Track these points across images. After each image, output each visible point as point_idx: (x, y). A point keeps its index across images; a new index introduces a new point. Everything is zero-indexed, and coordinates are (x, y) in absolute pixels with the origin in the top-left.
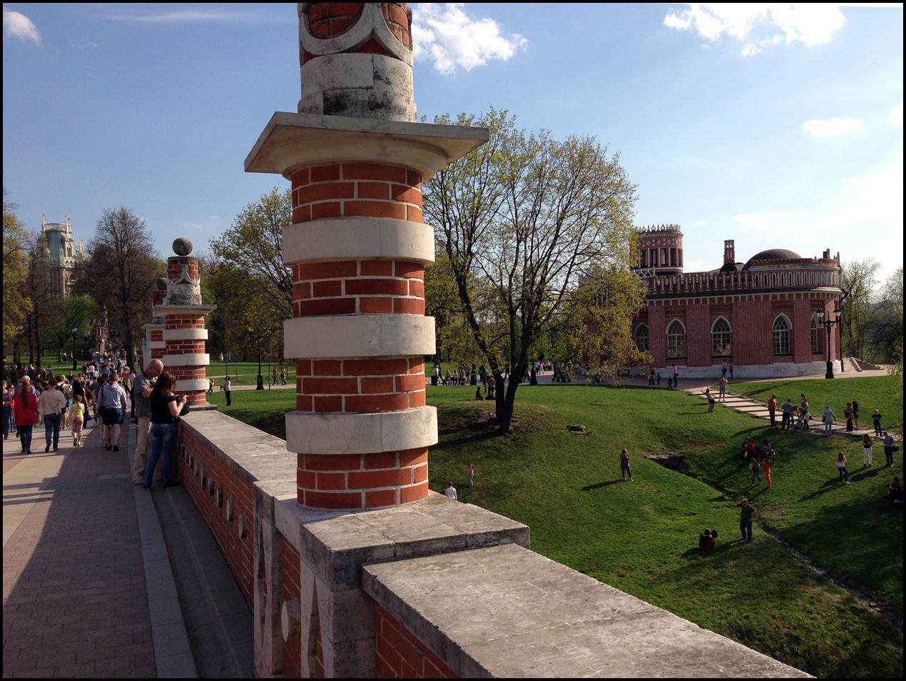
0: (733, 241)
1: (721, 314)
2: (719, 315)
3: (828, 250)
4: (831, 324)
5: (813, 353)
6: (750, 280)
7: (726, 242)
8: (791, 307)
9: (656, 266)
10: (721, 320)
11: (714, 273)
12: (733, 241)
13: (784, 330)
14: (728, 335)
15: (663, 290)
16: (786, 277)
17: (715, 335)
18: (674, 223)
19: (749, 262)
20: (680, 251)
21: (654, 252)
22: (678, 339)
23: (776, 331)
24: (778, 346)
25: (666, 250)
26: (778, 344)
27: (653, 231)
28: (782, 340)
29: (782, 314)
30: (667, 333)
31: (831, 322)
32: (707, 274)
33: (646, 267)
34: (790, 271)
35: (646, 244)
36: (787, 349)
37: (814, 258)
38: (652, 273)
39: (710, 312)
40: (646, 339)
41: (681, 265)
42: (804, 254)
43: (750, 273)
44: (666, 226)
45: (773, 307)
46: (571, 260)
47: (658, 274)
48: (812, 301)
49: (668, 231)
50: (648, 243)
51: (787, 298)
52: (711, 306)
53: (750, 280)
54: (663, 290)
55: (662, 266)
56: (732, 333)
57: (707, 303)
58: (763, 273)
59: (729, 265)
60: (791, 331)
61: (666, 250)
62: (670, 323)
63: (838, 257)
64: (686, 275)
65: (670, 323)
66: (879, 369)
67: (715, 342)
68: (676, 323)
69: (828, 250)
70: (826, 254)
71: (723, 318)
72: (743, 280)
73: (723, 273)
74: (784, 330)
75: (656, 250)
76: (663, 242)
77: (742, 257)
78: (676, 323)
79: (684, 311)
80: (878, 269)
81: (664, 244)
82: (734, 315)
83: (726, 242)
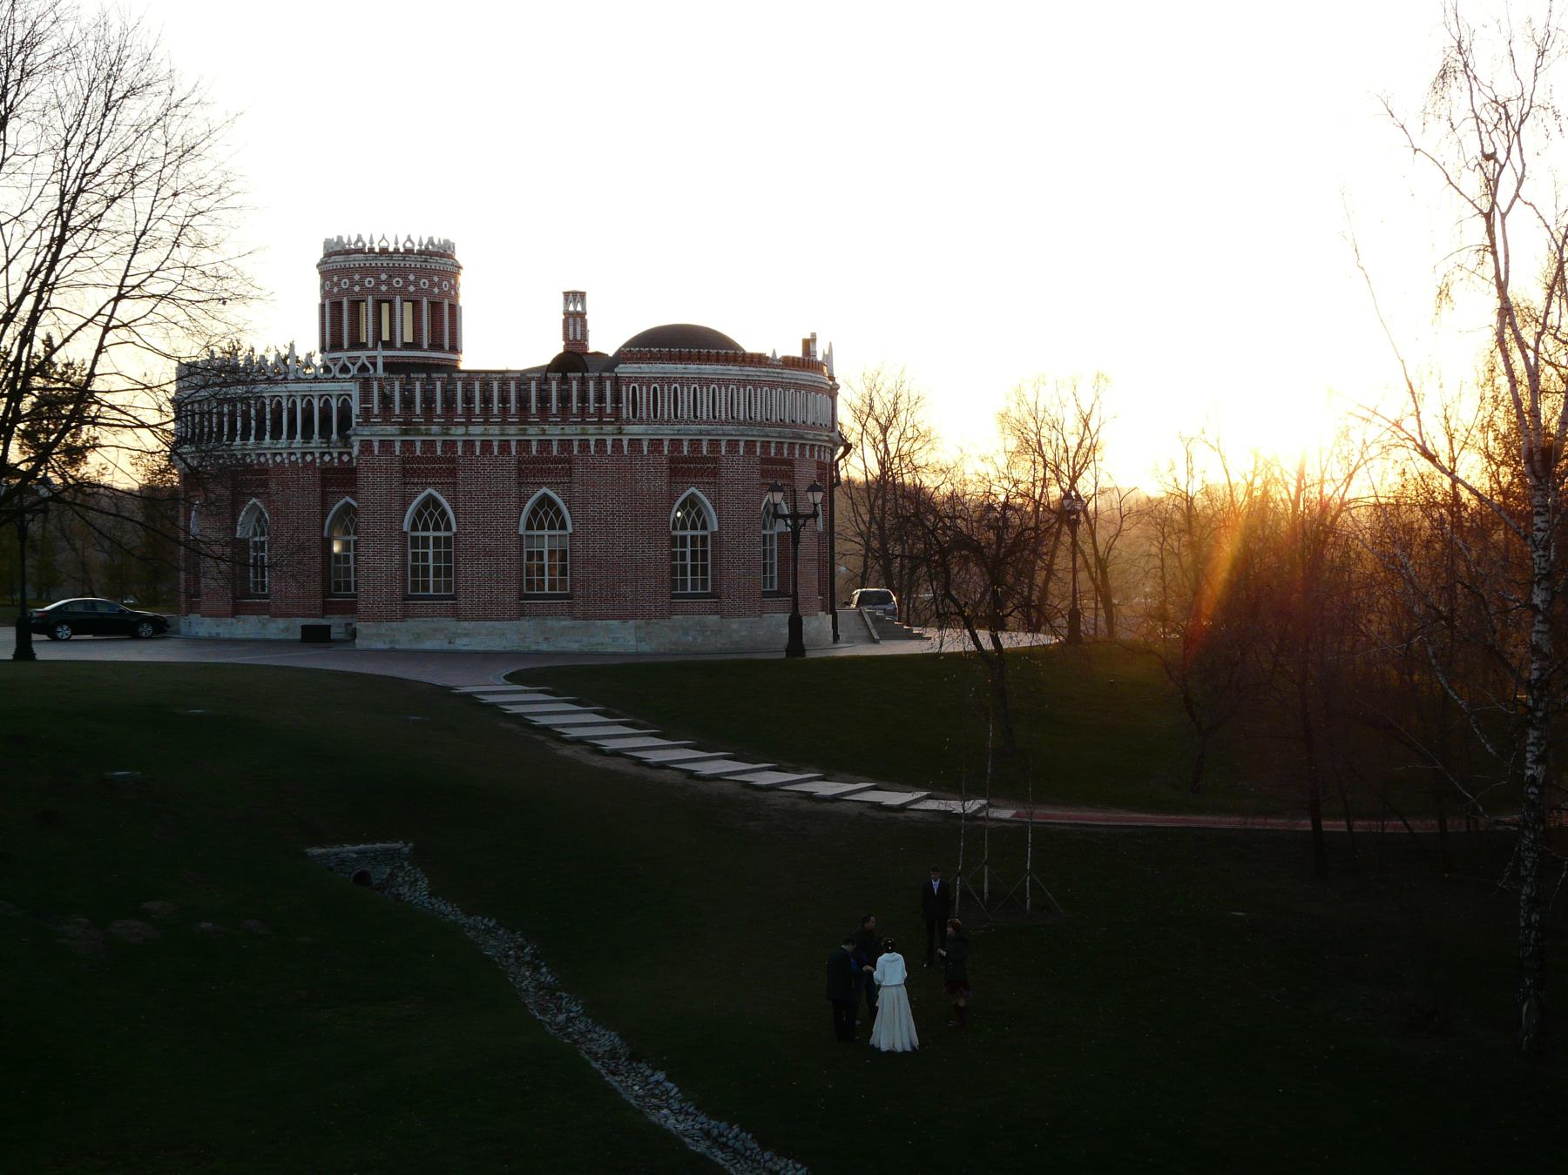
0: (583, 295)
1: (549, 485)
2: (540, 485)
3: (814, 335)
4: (801, 521)
5: (766, 595)
6: (617, 399)
7: (566, 294)
8: (715, 473)
9: (389, 345)
10: (545, 497)
11: (523, 378)
12: (583, 295)
13: (442, 534)
14: (447, 539)
15: (397, 411)
16: (705, 396)
17: (415, 539)
18: (439, 237)
19: (619, 352)
20: (454, 309)
21: (385, 307)
22: (694, 543)
23: (420, 534)
24: (684, 573)
25: (416, 305)
26: (684, 567)
27: (384, 251)
28: (694, 558)
29: (545, 490)
30: (406, 527)
31: (800, 516)
32: (504, 377)
33: (364, 346)
34: (712, 381)
35: (362, 285)
36: (704, 582)
37: (769, 354)
38: (374, 365)
39: (671, 477)
40: (355, 541)
41: (455, 348)
42: (750, 346)
43: (617, 382)
44: (416, 243)
45: (673, 472)
46: (108, 310)
47: (390, 366)
48: (766, 460)
49: (420, 253)
50: (370, 282)
51: (705, 452)
52: (672, 460)
53: (617, 399)
54: (397, 411)
55: (406, 346)
56: (455, 534)
57: (509, 453)
58: (648, 382)
59: (574, 359)
60: (712, 533)
61: (340, 304)
62: (415, 502)
63: (829, 357)
64: (472, 375)
65: (415, 502)
66: (919, 637)
67: (415, 555)
68: (431, 502)
69: (814, 335)
70: (808, 344)
71: (696, 491)
72: (600, 398)
73: (549, 375)
74: (699, 533)
75: (391, 303)
76: (407, 283)
77: (605, 339)
78: (431, 502)
79: (453, 473)
80: (294, 343)
81: (436, 290)
82: (577, 488)
83: (566, 294)
